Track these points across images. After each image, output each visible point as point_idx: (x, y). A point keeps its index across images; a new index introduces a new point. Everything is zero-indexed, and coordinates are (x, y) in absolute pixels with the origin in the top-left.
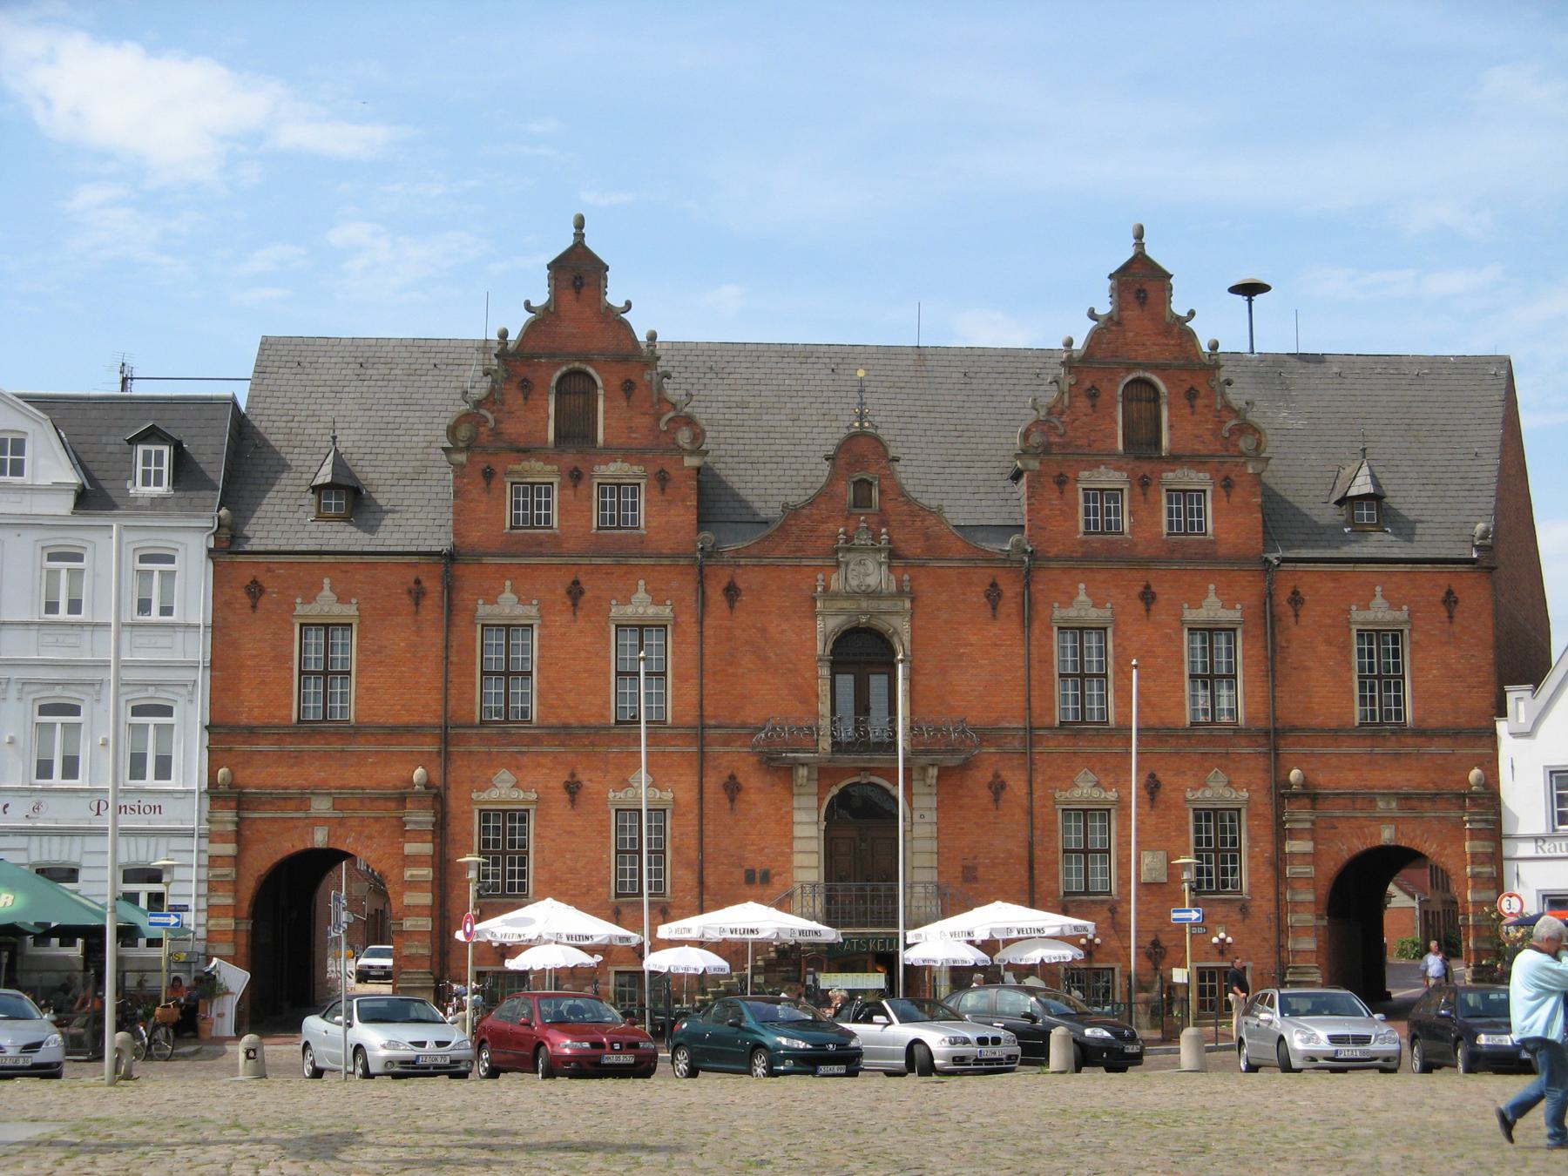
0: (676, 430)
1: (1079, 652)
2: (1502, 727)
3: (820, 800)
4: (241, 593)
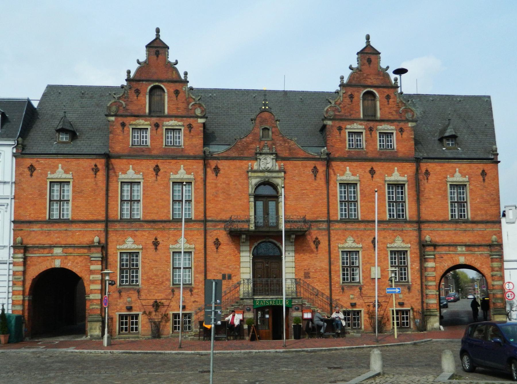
0: (195, 109)
3: (251, 248)
4: (26, 170)
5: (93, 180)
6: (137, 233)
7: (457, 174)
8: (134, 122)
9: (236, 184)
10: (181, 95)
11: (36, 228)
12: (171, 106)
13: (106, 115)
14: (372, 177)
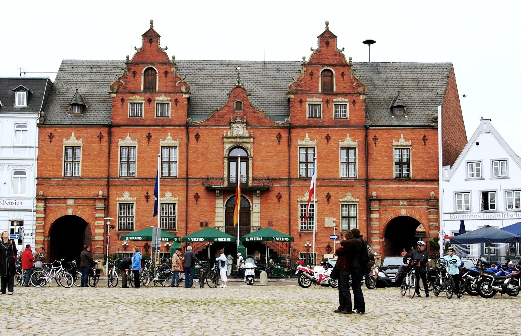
1: (401, 156)
3: (224, 201)
4: (47, 137)
6: (133, 188)
7: (402, 139)
10: (169, 75)
12: (162, 85)
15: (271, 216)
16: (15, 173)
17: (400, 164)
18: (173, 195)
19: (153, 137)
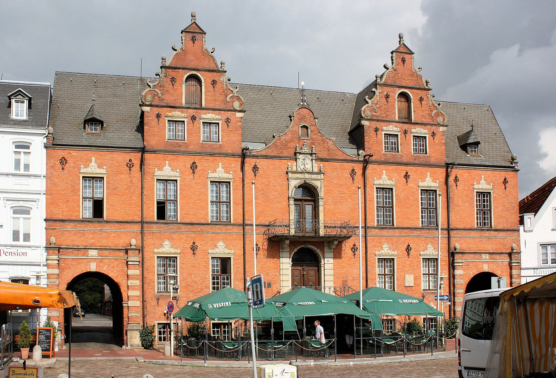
0: (233, 101)
1: (218, 193)
2: (521, 228)
3: (290, 254)
4: (58, 163)
5: (128, 176)
6: (175, 236)
7: (483, 181)
8: (169, 114)
9: (275, 186)
10: (218, 86)
11: (69, 227)
12: (208, 98)
13: (140, 105)
14: (407, 182)
15: (345, 273)
16: (15, 212)
17: (218, 202)
18: (227, 247)
19: (198, 168)
